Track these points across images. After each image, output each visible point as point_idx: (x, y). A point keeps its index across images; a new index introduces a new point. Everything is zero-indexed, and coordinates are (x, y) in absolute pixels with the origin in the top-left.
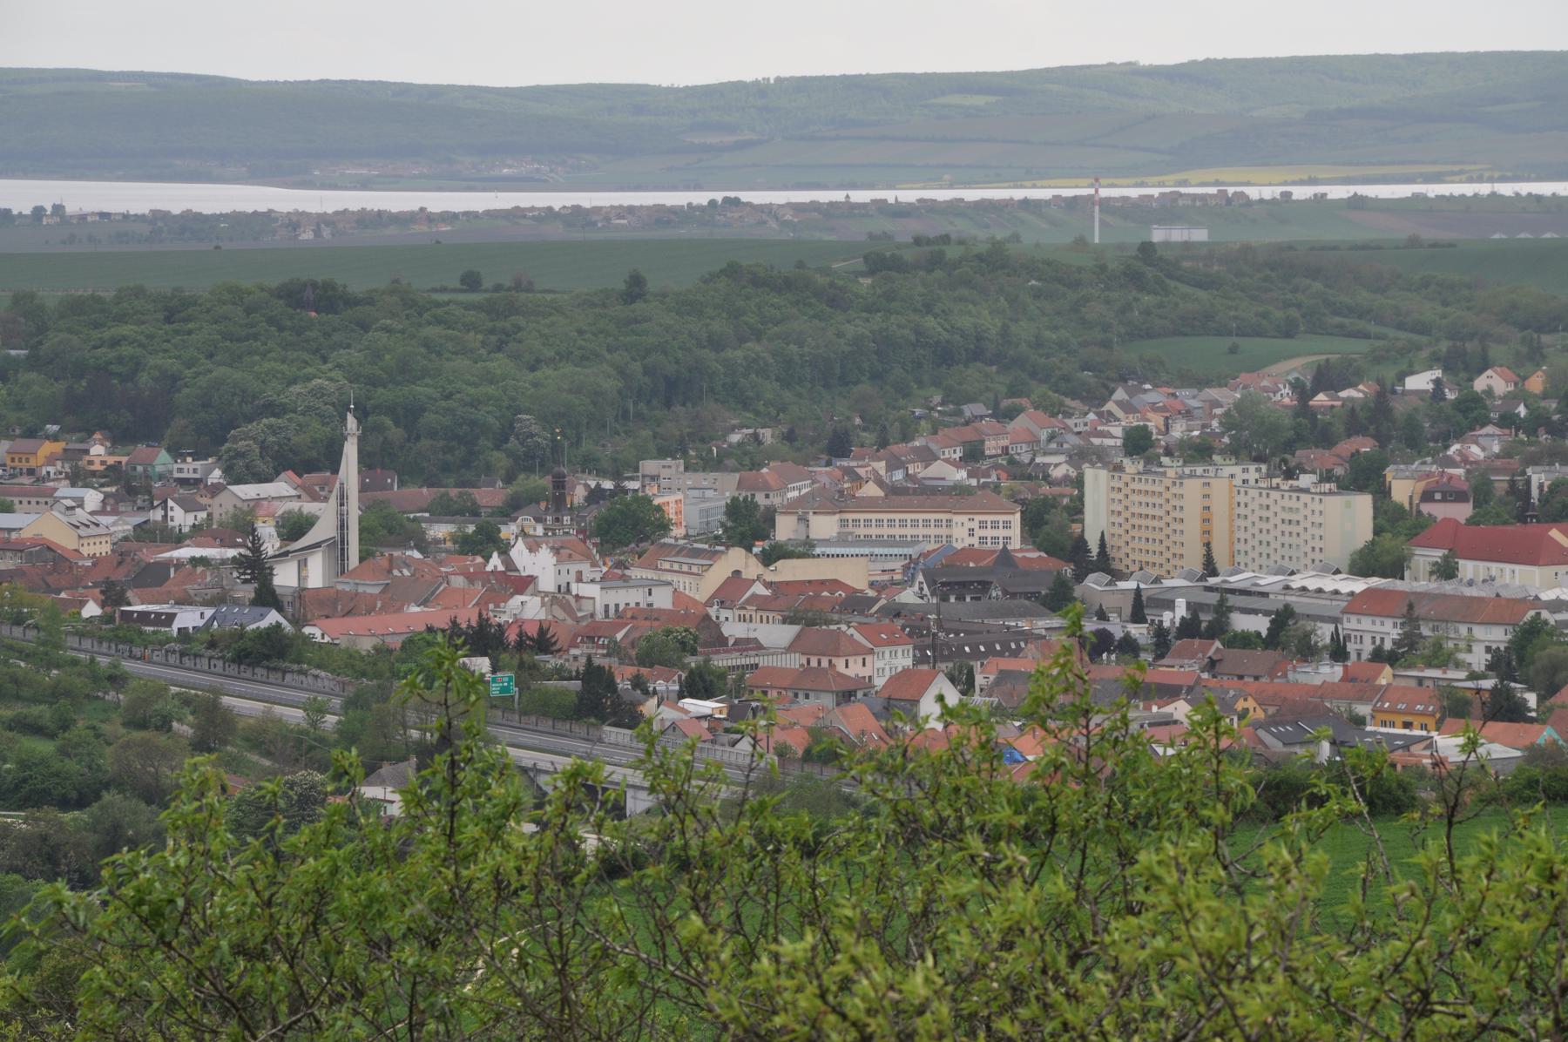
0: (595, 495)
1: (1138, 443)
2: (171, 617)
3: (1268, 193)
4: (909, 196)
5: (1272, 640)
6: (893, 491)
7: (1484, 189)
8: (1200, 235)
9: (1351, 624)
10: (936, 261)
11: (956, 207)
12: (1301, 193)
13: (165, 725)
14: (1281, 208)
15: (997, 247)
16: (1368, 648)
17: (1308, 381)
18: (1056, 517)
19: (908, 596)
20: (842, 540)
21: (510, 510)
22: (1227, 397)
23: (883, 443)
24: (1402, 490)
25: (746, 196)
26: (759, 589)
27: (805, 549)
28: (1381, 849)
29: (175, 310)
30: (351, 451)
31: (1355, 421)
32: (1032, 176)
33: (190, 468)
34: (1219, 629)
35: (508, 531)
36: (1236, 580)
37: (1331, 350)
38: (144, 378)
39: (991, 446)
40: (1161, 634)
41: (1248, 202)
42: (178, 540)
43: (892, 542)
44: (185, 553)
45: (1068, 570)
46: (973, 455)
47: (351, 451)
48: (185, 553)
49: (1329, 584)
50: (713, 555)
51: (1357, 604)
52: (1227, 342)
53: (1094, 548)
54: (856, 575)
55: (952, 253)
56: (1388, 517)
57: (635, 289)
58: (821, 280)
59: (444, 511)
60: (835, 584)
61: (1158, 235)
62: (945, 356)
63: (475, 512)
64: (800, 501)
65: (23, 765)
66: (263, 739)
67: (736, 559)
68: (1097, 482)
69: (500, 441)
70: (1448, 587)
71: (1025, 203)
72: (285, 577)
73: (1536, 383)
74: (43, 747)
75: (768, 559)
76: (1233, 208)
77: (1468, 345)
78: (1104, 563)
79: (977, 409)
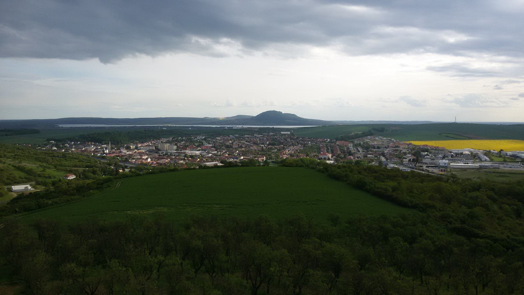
2: (98, 155)
3: (170, 126)
4: (147, 125)
5: (170, 155)
8: (166, 128)
9: (175, 154)
12: (172, 126)
15: (15, 166)
21: (120, 147)
22: (168, 139)
27: (140, 149)
28: (345, 147)
30: (110, 143)
31: (176, 141)
32: (155, 124)
34: (167, 154)
35: (120, 148)
36: (168, 151)
39: (152, 142)
40: (163, 155)
42: (98, 149)
43: (146, 149)
44: (99, 150)
45: (157, 151)
47: (110, 143)
49: (174, 151)
51: (176, 153)
54: (143, 151)
55: (150, 130)
56: (178, 147)
57: (129, 132)
58: (141, 132)
61: (163, 128)
66: (104, 163)
67: (136, 150)
68: (159, 145)
73: (186, 138)
74: (89, 164)
75: (138, 150)
76: (167, 127)
77: (140, 145)
78: (160, 150)
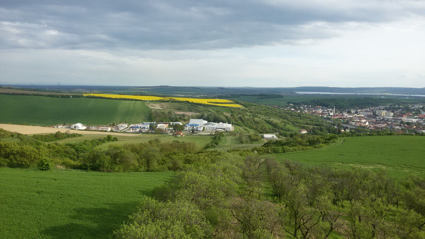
0: (348, 110)
1: (379, 109)
3: (388, 95)
6: (365, 111)
7: (401, 95)
10: (368, 98)
11: (369, 95)
13: (324, 122)
14: (388, 96)
16: (393, 121)
17: (390, 106)
18: (375, 113)
19: (366, 117)
20: (362, 114)
23: (364, 108)
24: (395, 112)
25: (357, 94)
26: (357, 116)
29: (326, 100)
30: (334, 108)
33: (326, 108)
34: (384, 120)
35: (343, 112)
36: (385, 117)
37: (391, 104)
38: (324, 103)
39: (371, 109)
41: (387, 95)
42: (325, 112)
44: (325, 112)
46: (370, 109)
47: (334, 108)
48: (325, 112)
49: (391, 118)
50: (354, 114)
51: (392, 119)
52: (385, 103)
53: (377, 115)
54: (362, 116)
57: (351, 99)
59: (339, 111)
60: (361, 116)
62: (368, 103)
63: (341, 111)
64: (360, 111)
65: (317, 124)
67: (356, 115)
68: (377, 111)
69: (343, 107)
70: (398, 118)
71: (374, 95)
72: (331, 114)
73: (403, 106)
76: (385, 96)
79: (370, 106)
